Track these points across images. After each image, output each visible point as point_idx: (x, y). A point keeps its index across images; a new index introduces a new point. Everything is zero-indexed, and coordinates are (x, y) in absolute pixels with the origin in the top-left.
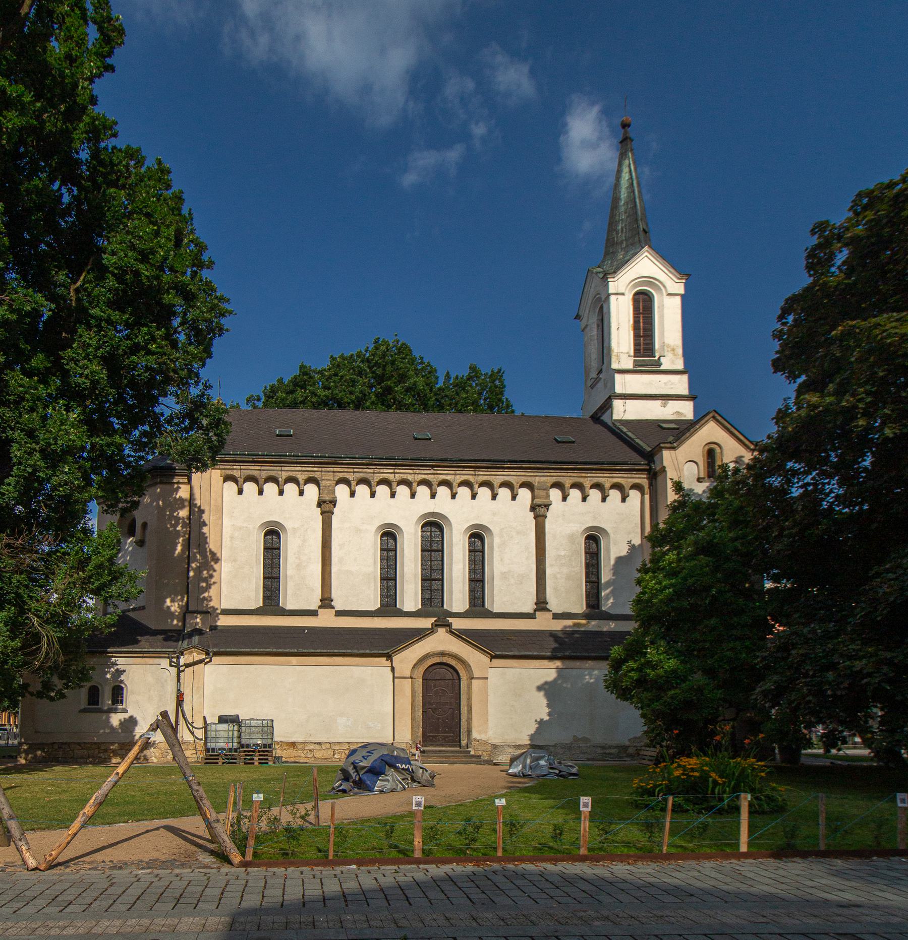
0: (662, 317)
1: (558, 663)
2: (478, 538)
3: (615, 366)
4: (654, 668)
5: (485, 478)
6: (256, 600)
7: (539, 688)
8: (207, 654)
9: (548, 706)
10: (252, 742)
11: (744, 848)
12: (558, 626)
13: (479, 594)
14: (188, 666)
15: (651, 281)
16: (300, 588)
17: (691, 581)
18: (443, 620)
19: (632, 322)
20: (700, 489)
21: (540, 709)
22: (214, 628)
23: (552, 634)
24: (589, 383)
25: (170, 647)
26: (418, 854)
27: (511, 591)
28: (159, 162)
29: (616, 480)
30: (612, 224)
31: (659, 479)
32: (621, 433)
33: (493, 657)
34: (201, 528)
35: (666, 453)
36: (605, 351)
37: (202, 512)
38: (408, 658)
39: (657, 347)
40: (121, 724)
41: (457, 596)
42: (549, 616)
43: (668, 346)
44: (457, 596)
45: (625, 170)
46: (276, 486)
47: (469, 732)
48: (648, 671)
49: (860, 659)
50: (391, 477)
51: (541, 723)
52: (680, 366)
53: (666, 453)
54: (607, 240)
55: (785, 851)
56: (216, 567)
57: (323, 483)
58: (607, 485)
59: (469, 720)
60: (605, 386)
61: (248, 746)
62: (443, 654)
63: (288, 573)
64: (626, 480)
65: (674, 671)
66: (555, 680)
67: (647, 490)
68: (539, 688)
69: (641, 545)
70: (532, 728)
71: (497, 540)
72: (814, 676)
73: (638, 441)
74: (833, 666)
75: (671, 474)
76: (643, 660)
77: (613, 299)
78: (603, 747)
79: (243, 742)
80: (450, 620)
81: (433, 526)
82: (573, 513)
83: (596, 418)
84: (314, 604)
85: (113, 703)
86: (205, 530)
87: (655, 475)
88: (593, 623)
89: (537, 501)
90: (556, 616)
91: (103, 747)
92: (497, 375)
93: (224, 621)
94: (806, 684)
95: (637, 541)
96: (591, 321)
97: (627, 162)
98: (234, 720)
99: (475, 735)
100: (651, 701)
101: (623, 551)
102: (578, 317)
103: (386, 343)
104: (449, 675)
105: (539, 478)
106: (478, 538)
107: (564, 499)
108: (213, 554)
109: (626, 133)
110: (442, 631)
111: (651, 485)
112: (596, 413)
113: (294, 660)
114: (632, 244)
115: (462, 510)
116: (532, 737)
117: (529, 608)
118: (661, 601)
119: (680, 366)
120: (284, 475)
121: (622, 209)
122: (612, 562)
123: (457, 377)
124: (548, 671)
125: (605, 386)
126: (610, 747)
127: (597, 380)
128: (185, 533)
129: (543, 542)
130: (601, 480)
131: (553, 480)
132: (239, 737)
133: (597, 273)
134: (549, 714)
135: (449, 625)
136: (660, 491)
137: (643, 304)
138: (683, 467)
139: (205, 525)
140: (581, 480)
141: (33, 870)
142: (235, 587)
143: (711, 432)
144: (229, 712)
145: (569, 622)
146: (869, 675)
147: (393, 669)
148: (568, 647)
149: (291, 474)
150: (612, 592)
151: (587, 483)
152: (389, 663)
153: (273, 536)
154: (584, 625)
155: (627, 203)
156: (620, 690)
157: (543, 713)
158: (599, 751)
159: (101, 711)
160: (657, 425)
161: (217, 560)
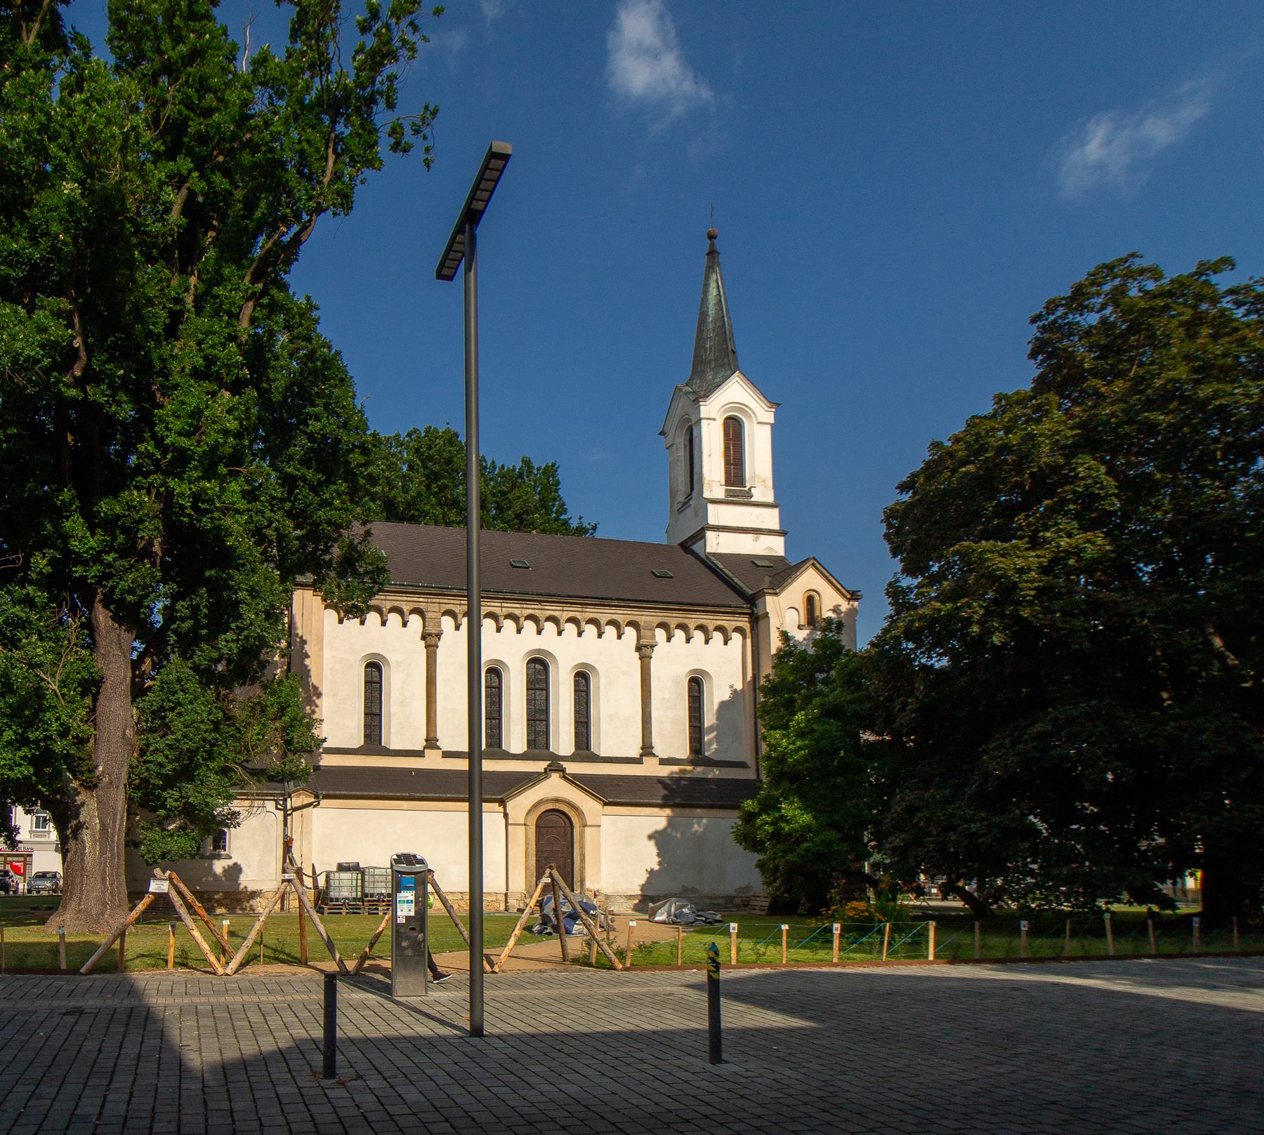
0: (752, 445)
1: (668, 811)
2: (582, 678)
3: (706, 495)
4: (788, 822)
5: (592, 615)
6: (358, 740)
7: (650, 837)
8: (317, 797)
9: (659, 855)
10: (377, 891)
11: (931, 958)
12: (664, 771)
13: (495, 708)
14: (295, 809)
15: (742, 407)
16: (403, 728)
17: (824, 743)
18: (555, 765)
19: (723, 449)
20: (800, 636)
21: (650, 858)
22: (317, 768)
23: (660, 781)
24: (676, 507)
25: (277, 789)
26: (734, 962)
27: (616, 735)
28: (308, 299)
29: (719, 623)
30: (700, 340)
31: (761, 623)
32: (714, 567)
33: (605, 804)
34: (303, 660)
35: (769, 599)
36: (695, 477)
37: (304, 642)
38: (521, 804)
39: (747, 476)
40: (225, 871)
41: (563, 740)
42: (656, 761)
43: (759, 477)
44: (563, 740)
45: (713, 285)
46: (378, 615)
47: (582, 881)
48: (783, 825)
49: (974, 822)
50: (498, 611)
51: (651, 872)
52: (770, 498)
53: (769, 599)
54: (695, 356)
55: (954, 960)
56: (318, 702)
57: (428, 615)
58: (711, 628)
59: (582, 869)
60: (696, 514)
61: (372, 895)
62: (556, 800)
63: (392, 710)
64: (729, 622)
65: (809, 826)
66: (665, 829)
67: (749, 634)
68: (650, 837)
69: (743, 690)
70: (643, 878)
71: (603, 681)
72: (937, 835)
73: (736, 580)
74: (953, 828)
75: (774, 622)
76: (777, 815)
77: (704, 423)
78: (711, 898)
79: (367, 891)
80: (565, 764)
81: (539, 667)
82: (677, 656)
83: (686, 546)
84: (419, 745)
85: (215, 849)
86: (307, 662)
87: (758, 620)
88: (699, 769)
89: (643, 642)
90: (664, 762)
91: (206, 896)
92: (550, 471)
93: (327, 761)
94: (932, 842)
95: (739, 686)
96: (677, 441)
97: (714, 277)
98: (355, 868)
99: (588, 885)
100: (785, 852)
101: (726, 696)
102: (662, 433)
103: (436, 430)
104: (561, 821)
105: (644, 617)
106: (582, 678)
107: (669, 640)
108: (315, 688)
109: (712, 245)
110: (555, 777)
111: (752, 629)
112: (685, 541)
113: (405, 804)
114: (722, 366)
115: (569, 648)
116: (643, 887)
117: (635, 752)
118: (796, 761)
119: (770, 498)
120: (389, 605)
121: (710, 327)
122: (716, 707)
123: (503, 467)
124: (657, 819)
125: (696, 514)
126: (717, 897)
127: (686, 504)
128: (283, 664)
129: (652, 685)
130: (704, 622)
131: (659, 620)
132: (363, 886)
133: (687, 393)
134: (660, 863)
135: (563, 770)
136: (761, 636)
137: (734, 429)
138: (784, 614)
139: (308, 656)
140: (686, 621)
141: (575, 961)
142: (338, 722)
143: (809, 579)
144: (345, 859)
145: (676, 768)
146: (983, 836)
147: (506, 816)
148: (679, 794)
149: (396, 604)
150: (716, 737)
151: (692, 625)
152: (501, 809)
153: (374, 669)
154: (689, 772)
155: (715, 321)
156: (749, 840)
157: (653, 862)
158: (707, 901)
159: (203, 857)
160: (750, 562)
161: (319, 695)
